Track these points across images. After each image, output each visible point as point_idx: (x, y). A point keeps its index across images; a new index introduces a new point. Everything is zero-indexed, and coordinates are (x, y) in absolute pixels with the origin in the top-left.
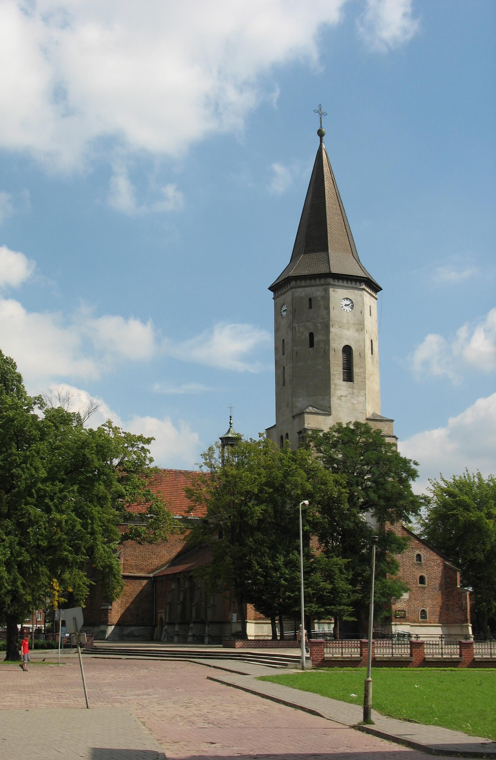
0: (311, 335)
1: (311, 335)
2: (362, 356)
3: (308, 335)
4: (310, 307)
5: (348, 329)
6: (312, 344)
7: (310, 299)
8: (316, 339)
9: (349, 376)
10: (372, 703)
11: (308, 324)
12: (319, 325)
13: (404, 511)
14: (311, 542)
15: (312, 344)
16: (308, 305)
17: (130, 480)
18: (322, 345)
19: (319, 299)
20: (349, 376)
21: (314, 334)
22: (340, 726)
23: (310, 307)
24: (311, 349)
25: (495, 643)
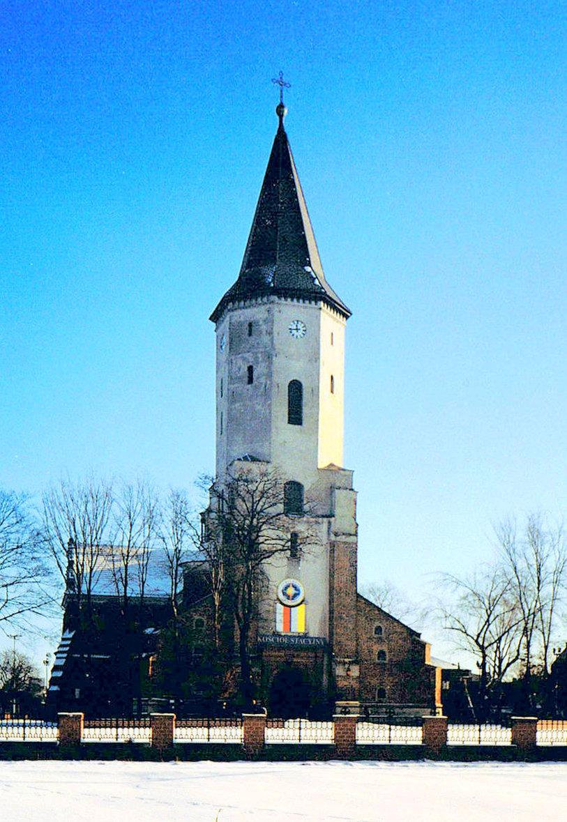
0: (250, 369)
1: (250, 369)
2: (315, 392)
3: (246, 369)
4: (250, 334)
5: (298, 360)
6: (250, 381)
7: (250, 325)
8: (255, 374)
9: (295, 417)
10: (356, 700)
11: (246, 355)
12: (260, 355)
13: (487, 686)
14: (508, 681)
15: (250, 381)
16: (247, 332)
17: (69, 579)
18: (263, 380)
19: (261, 323)
20: (295, 417)
21: (254, 367)
22: (546, 640)
23: (250, 334)
24: (250, 386)
25: (565, 722)
